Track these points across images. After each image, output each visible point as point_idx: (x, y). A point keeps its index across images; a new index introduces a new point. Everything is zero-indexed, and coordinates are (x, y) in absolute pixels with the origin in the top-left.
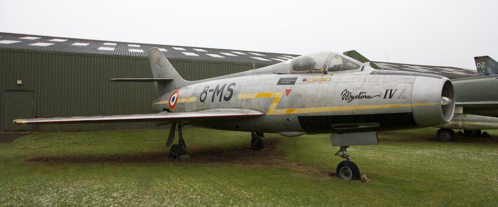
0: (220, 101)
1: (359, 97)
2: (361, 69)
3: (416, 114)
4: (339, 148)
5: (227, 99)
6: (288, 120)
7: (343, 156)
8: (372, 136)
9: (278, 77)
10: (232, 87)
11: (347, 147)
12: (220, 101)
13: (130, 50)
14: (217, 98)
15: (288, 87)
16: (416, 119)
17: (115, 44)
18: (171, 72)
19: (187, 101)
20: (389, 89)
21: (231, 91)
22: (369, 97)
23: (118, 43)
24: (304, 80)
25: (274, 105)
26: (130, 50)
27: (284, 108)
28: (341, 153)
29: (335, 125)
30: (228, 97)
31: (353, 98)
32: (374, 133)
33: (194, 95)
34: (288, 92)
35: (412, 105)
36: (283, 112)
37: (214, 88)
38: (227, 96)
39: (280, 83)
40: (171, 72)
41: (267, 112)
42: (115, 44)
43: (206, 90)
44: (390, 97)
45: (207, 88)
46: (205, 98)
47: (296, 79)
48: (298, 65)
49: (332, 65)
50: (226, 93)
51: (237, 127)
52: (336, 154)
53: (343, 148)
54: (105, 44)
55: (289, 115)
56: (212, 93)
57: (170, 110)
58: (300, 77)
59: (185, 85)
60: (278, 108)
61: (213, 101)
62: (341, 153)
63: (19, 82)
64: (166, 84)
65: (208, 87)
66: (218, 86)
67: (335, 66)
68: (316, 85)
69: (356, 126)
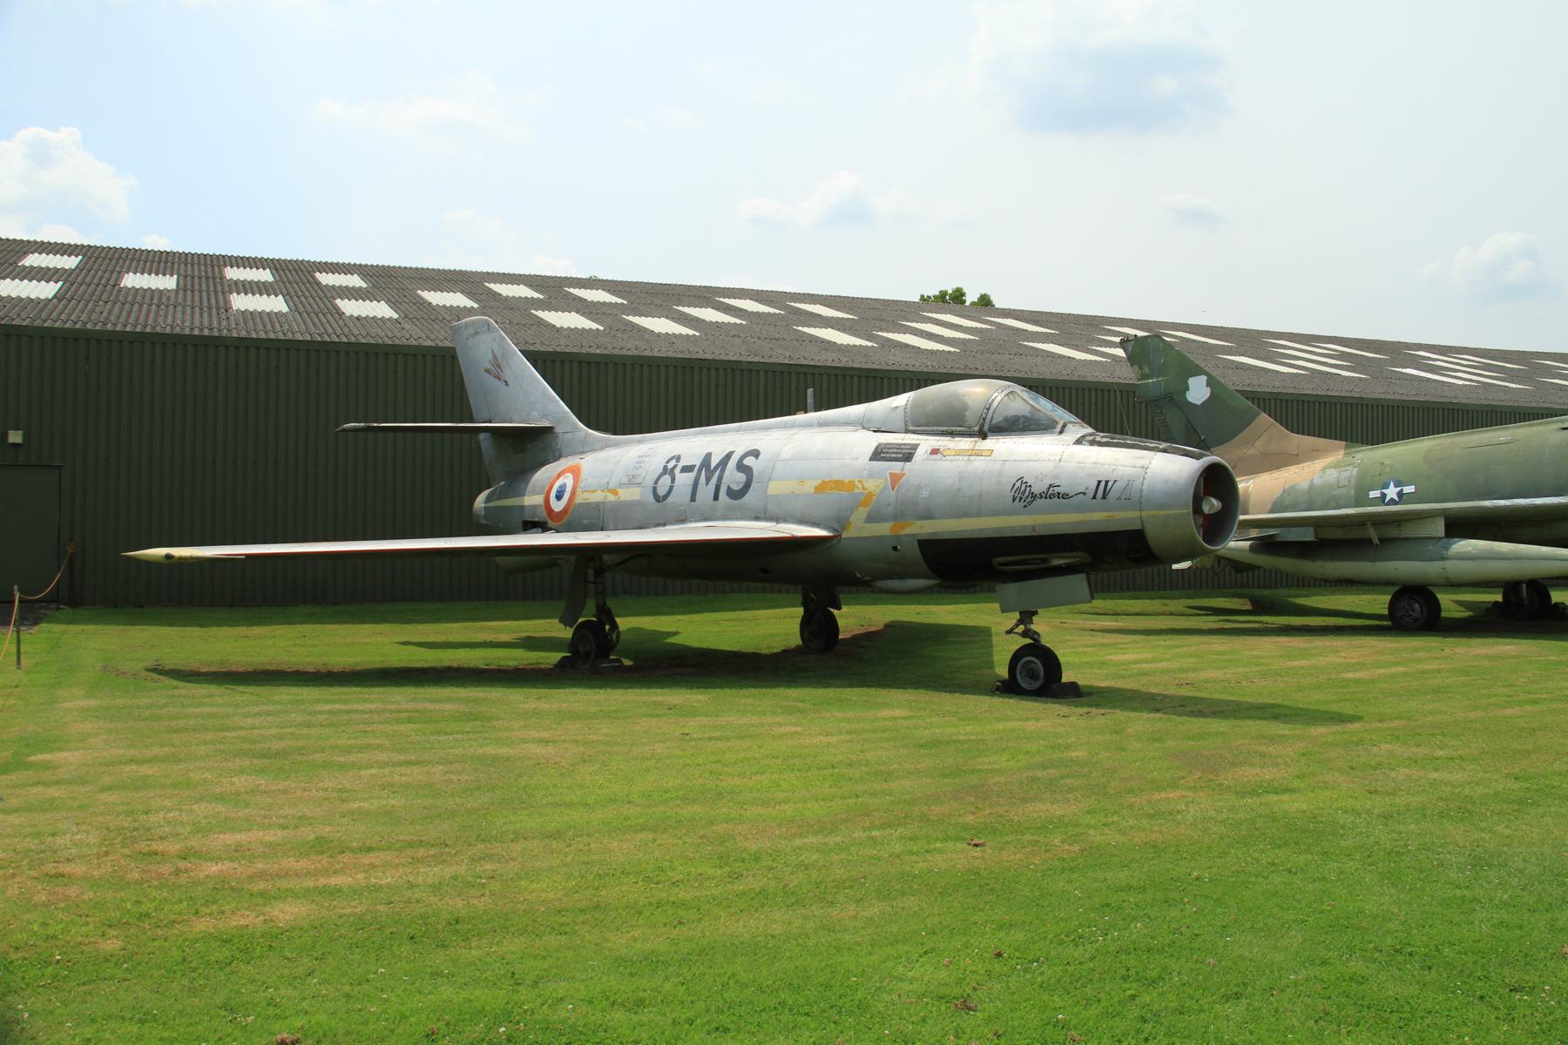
0: (716, 498)
1: (1046, 495)
2: (1058, 429)
3: (1151, 534)
4: (1017, 616)
5: (735, 495)
6: (895, 548)
7: (1025, 634)
8: (1079, 582)
9: (872, 440)
10: (749, 461)
11: (1035, 613)
12: (716, 498)
13: (240, 302)
14: (705, 492)
15: (896, 467)
16: (1152, 542)
17: (70, 262)
18: (534, 400)
19: (611, 497)
20: (1104, 479)
21: (747, 471)
22: (1065, 496)
23: (275, 265)
24: (935, 452)
25: (862, 512)
26: (240, 302)
27: (885, 520)
28: (1021, 628)
29: (1000, 560)
30: (736, 486)
31: (1034, 496)
32: (1083, 576)
33: (632, 482)
34: (895, 479)
35: (1145, 514)
36: (884, 529)
37: (697, 462)
38: (735, 487)
39: (879, 454)
40: (534, 400)
41: (844, 528)
42: (70, 262)
43: (670, 466)
44: (1104, 497)
45: (673, 463)
46: (671, 488)
47: (915, 447)
48: (1346, 447)
49: (998, 419)
50: (733, 477)
51: (764, 571)
52: (1010, 632)
53: (1027, 616)
54: (33, 260)
55: (898, 537)
56: (691, 476)
57: (551, 523)
58: (926, 443)
59: (584, 448)
60: (870, 519)
61: (693, 499)
62: (1021, 628)
63: (15, 437)
64: (530, 446)
65: (678, 458)
66: (709, 456)
67: (1006, 420)
68: (961, 462)
69: (1044, 560)
